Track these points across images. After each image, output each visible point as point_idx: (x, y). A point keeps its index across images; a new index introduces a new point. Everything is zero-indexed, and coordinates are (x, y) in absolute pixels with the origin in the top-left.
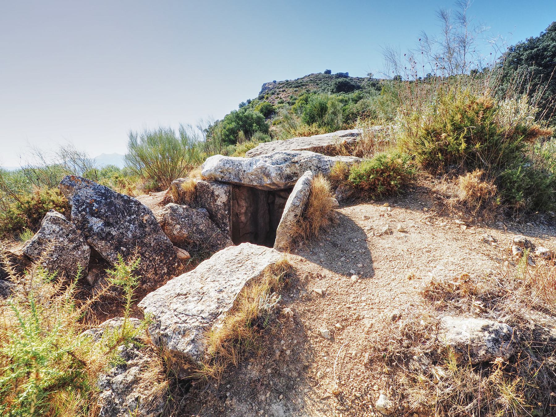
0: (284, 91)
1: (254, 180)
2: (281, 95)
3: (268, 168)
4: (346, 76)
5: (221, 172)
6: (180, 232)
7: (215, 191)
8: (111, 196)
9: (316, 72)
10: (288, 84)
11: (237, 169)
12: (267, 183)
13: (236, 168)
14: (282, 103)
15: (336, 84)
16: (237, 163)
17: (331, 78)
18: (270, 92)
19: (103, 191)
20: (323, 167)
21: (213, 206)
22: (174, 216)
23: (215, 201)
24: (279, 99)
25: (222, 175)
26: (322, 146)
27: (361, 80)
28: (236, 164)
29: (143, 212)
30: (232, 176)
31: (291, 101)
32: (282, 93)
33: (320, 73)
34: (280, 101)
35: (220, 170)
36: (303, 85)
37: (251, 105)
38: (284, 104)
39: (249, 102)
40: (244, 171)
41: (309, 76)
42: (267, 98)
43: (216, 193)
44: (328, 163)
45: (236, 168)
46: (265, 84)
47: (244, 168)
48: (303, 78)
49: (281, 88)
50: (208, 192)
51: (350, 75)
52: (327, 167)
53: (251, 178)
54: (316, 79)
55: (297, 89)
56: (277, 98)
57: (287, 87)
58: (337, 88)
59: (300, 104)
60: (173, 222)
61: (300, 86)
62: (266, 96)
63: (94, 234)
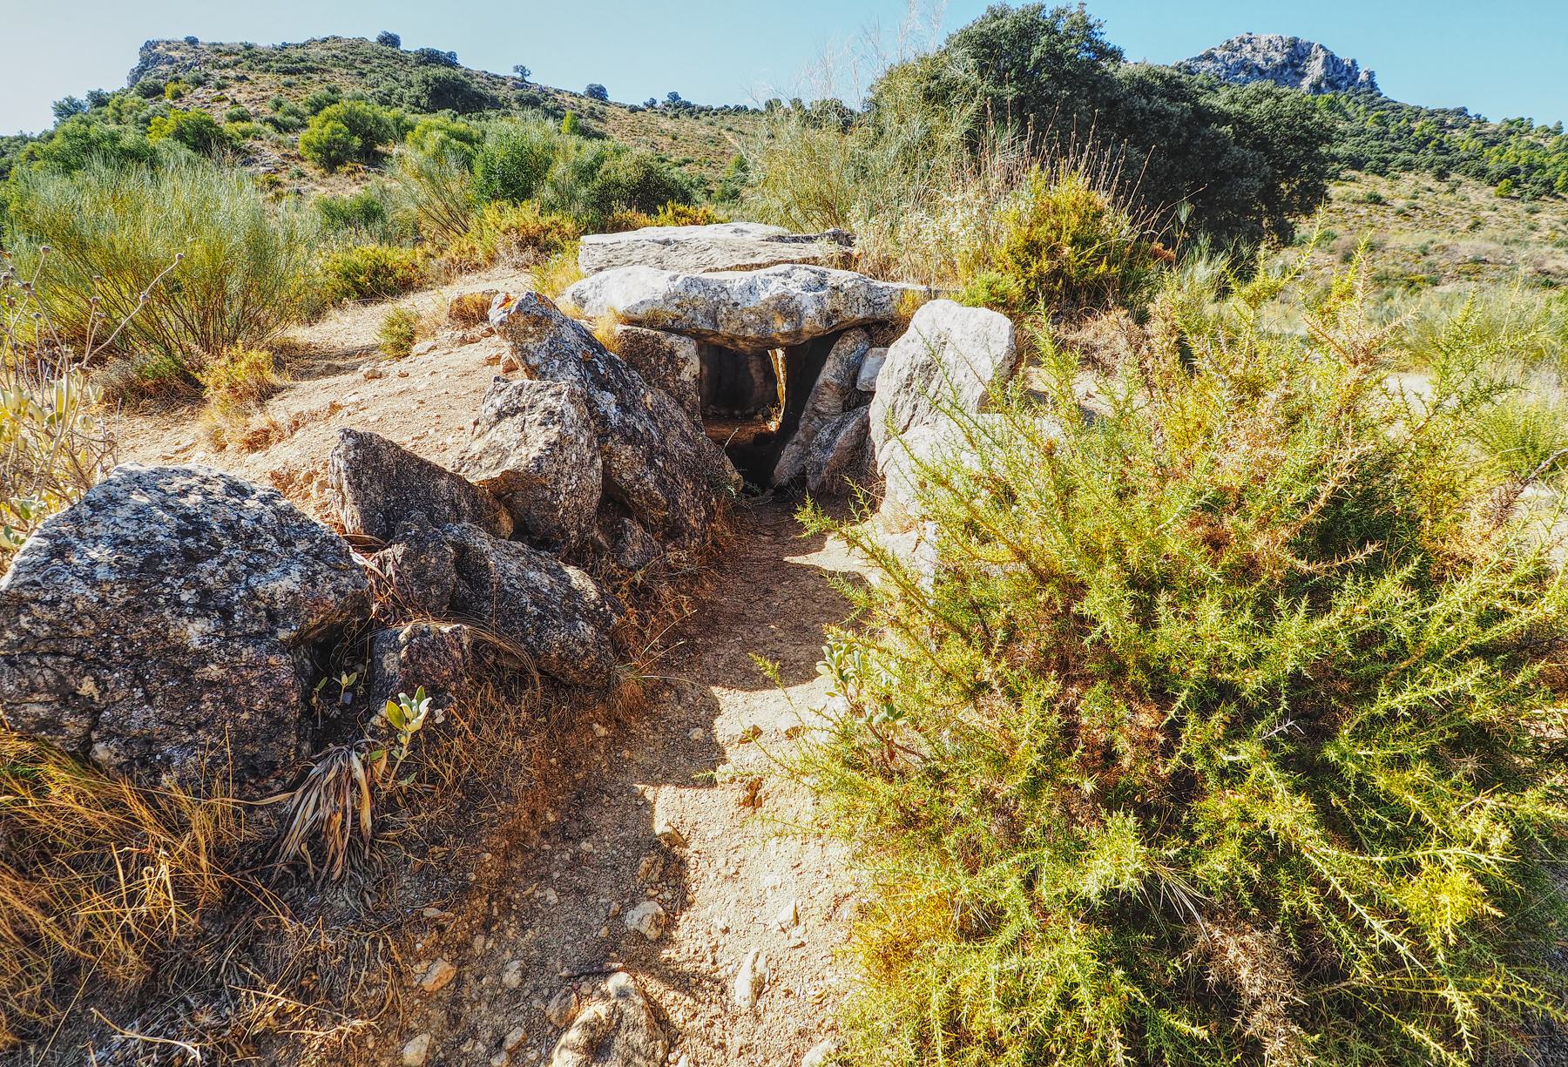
1: (753, 323)
2: (233, 91)
3: (798, 298)
4: (449, 61)
5: (678, 306)
7: (676, 348)
9: (348, 32)
10: (250, 55)
12: (782, 330)
13: (712, 298)
14: (243, 117)
15: (425, 82)
17: (403, 59)
18: (187, 76)
23: (679, 371)
24: (227, 104)
25: (679, 312)
31: (278, 116)
32: (237, 85)
33: (362, 41)
34: (234, 111)
35: (677, 301)
36: (311, 70)
37: (108, 111)
38: (255, 124)
39: (99, 100)
40: (736, 304)
41: (325, 41)
42: (178, 95)
43: (681, 354)
45: (712, 298)
46: (150, 45)
47: (736, 297)
48: (303, 46)
49: (226, 66)
50: (657, 353)
52: (884, 300)
53: (746, 319)
54: (352, 56)
55: (293, 79)
56: (220, 100)
57: (250, 68)
58: (431, 97)
59: (327, 130)
61: (300, 72)
62: (171, 87)
63: (613, 430)
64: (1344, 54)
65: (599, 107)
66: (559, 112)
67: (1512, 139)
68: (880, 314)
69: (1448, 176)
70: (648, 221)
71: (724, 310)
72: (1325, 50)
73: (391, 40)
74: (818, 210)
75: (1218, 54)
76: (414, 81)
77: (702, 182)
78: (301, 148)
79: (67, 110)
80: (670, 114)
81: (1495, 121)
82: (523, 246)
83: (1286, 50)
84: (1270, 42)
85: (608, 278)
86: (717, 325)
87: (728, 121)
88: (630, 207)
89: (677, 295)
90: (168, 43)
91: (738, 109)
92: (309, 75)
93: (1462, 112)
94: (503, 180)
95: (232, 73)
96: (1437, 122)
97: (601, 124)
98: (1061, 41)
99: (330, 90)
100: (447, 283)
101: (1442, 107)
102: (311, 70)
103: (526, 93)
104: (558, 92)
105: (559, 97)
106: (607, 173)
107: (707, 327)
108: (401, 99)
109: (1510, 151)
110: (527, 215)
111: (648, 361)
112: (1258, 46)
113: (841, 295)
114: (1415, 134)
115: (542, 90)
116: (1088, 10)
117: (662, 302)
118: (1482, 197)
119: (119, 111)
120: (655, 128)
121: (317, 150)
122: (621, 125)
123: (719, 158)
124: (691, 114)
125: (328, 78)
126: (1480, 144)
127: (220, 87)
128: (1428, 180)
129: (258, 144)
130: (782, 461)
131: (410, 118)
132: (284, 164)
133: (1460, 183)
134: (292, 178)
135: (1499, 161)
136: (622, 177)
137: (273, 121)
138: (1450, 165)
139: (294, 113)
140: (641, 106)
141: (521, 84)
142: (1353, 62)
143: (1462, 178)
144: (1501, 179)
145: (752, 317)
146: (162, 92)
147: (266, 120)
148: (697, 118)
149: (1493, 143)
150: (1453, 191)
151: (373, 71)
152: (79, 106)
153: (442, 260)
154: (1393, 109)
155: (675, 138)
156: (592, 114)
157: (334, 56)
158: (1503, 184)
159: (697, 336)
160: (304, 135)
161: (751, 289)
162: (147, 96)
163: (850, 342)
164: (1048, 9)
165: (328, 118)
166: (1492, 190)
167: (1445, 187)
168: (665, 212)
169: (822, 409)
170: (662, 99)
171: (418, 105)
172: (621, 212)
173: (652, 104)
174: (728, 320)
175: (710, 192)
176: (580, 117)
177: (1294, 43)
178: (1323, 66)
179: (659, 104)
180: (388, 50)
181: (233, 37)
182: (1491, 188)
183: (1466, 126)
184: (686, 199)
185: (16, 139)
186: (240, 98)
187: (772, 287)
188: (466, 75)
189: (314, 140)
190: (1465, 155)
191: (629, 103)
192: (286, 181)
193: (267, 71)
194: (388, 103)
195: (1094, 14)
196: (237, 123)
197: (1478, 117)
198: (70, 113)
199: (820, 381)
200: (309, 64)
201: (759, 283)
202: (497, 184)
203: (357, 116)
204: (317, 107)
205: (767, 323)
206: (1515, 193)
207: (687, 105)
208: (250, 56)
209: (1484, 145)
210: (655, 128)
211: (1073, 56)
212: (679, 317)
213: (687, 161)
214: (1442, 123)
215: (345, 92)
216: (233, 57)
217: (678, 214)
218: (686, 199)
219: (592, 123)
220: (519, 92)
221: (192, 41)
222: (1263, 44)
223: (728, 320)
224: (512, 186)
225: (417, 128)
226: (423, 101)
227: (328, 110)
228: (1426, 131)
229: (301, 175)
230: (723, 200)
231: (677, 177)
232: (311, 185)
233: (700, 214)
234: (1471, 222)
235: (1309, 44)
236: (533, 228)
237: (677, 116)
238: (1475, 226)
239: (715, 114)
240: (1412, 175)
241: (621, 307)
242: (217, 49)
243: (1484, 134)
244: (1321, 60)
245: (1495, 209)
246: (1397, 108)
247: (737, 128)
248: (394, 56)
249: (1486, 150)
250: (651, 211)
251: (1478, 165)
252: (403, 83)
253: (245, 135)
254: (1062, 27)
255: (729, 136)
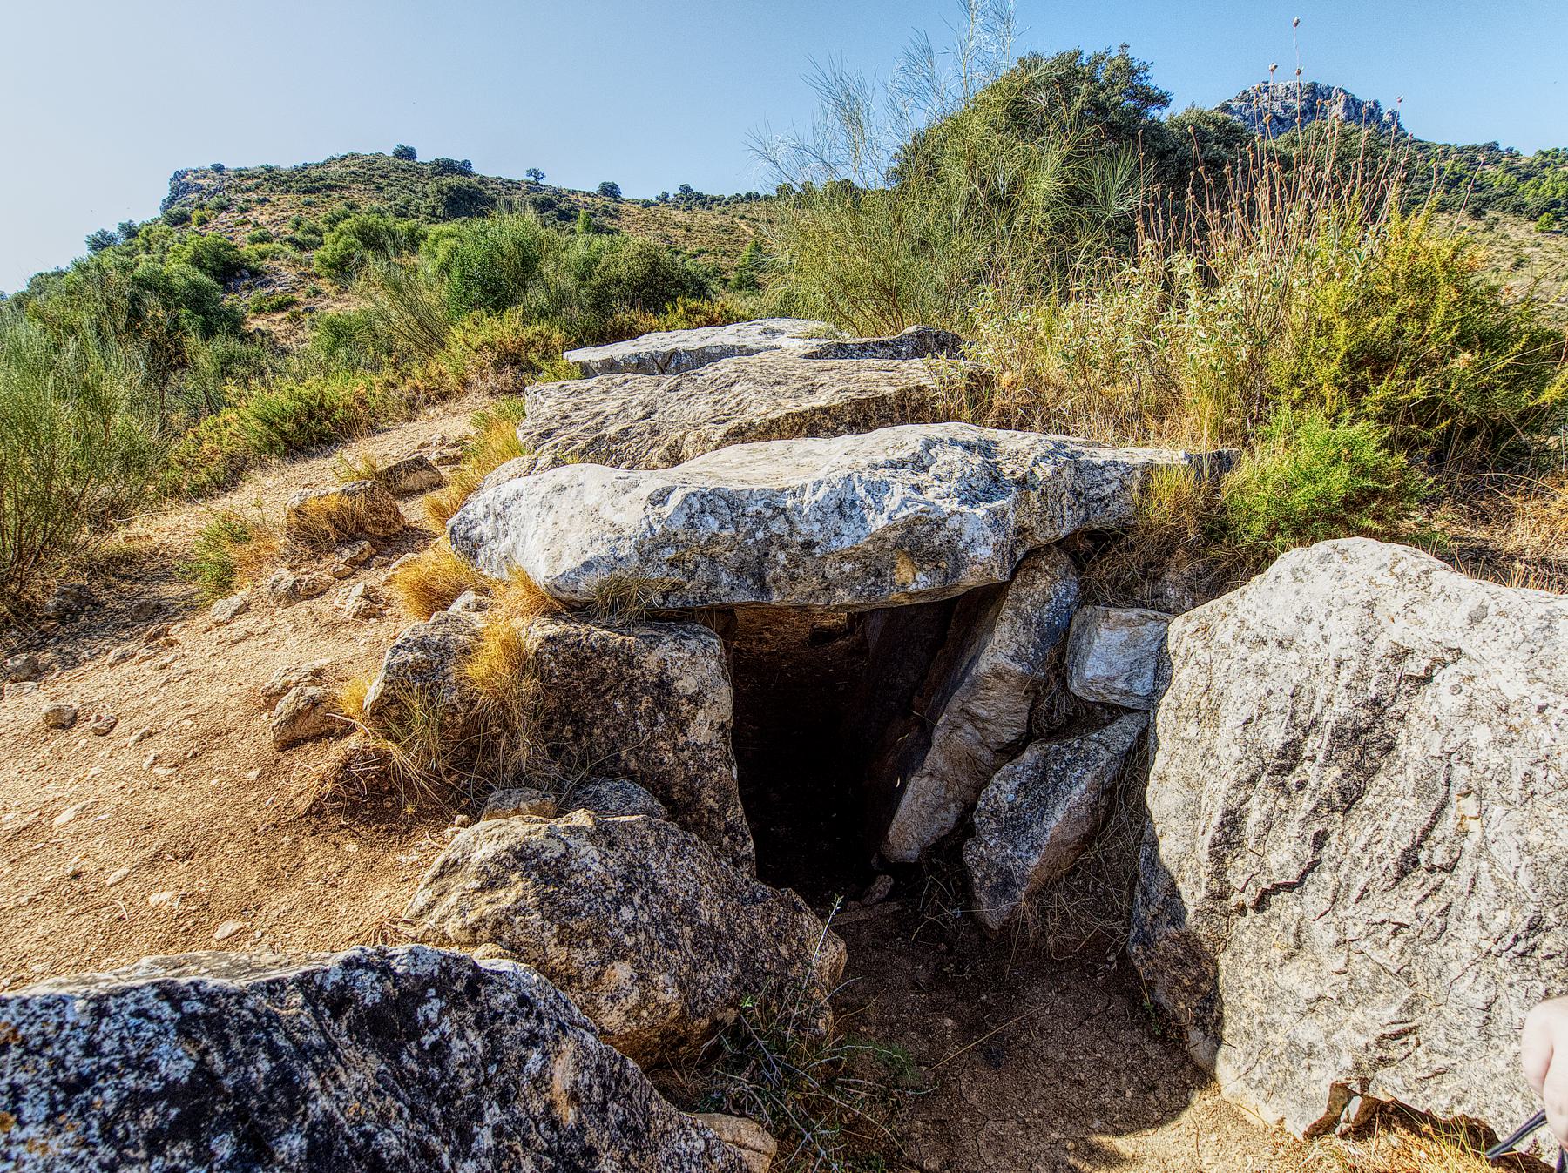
0: (265, 200)
2: (255, 214)
4: (464, 169)
6: (644, 1001)
8: (284, 1080)
9: (366, 150)
10: (272, 178)
11: (760, 535)
13: (751, 533)
14: (265, 239)
15: (440, 191)
16: (759, 506)
18: (210, 203)
19: (176, 1064)
20: (1091, 492)
21: (668, 757)
22: (572, 912)
23: (683, 726)
24: (250, 227)
25: (678, 576)
26: (884, 397)
27: (510, 186)
28: (751, 510)
29: (532, 1040)
30: (724, 578)
31: (298, 235)
32: (259, 207)
33: (379, 156)
34: (256, 233)
35: (669, 553)
36: (330, 188)
37: (138, 241)
38: (276, 245)
39: (130, 231)
40: (808, 545)
41: (343, 159)
42: (203, 222)
43: (687, 685)
44: (1112, 474)
45: (751, 533)
46: (179, 175)
48: (323, 165)
49: (248, 190)
51: (474, 168)
53: (832, 573)
54: (370, 172)
55: (313, 198)
56: (243, 224)
57: (271, 190)
59: (340, 245)
60: (578, 955)
61: (319, 190)
62: (198, 213)
64: (1364, 95)
65: (612, 205)
66: (573, 212)
67: (1547, 172)
68: (1099, 520)
69: (1485, 213)
70: (655, 322)
71: (782, 558)
72: (1345, 93)
73: (407, 153)
74: (873, 298)
75: (1233, 105)
76: (429, 192)
77: (718, 271)
78: (316, 266)
79: (100, 243)
80: (682, 206)
81: (1528, 153)
82: (499, 366)
83: (1305, 97)
84: (1288, 89)
85: (518, 495)
86: (764, 590)
87: (741, 209)
88: (632, 306)
89: (669, 540)
90: (196, 172)
91: (749, 196)
92: (329, 193)
93: (1493, 147)
94: (483, 286)
95: (254, 197)
96: (1467, 160)
97: (616, 222)
98: (1102, 88)
99: (348, 206)
100: (409, 419)
101: (1471, 143)
102: (330, 188)
103: (540, 196)
104: (572, 192)
105: (573, 198)
106: (607, 267)
107: (744, 597)
108: (417, 210)
109: (1547, 184)
110: (506, 328)
111: (608, 708)
112: (1275, 94)
113: (1033, 495)
114: (1446, 173)
115: (555, 192)
116: (1131, 53)
117: (634, 562)
118: (1522, 234)
119: (148, 241)
120: (669, 221)
121: (332, 266)
122: (635, 221)
123: (734, 247)
124: (703, 204)
125: (347, 194)
126: (1514, 179)
127: (243, 211)
128: (1463, 219)
129: (275, 264)
130: (902, 812)
131: (425, 227)
132: (300, 282)
133: (1497, 220)
134: (309, 296)
135: (1536, 195)
136: (624, 272)
137: (292, 241)
138: (1486, 202)
139: (314, 231)
140: (654, 200)
141: (535, 187)
142: (1376, 104)
143: (1500, 215)
144: (1541, 213)
145: (847, 567)
146: (189, 219)
147: (286, 240)
148: (710, 208)
149: (1528, 177)
150: (1491, 229)
151: (390, 185)
152: (112, 239)
153: (405, 389)
154: (1420, 149)
155: (688, 230)
156: (605, 213)
157: (352, 172)
158: (1543, 218)
159: (724, 620)
160: (321, 252)
161: (844, 507)
162: (175, 224)
163: (1042, 583)
164: (1085, 56)
165: (342, 234)
166: (1532, 225)
167: (1481, 225)
168: (675, 309)
169: (983, 713)
170: (673, 191)
171: (435, 215)
172: (623, 315)
173: (664, 198)
174: (792, 578)
175: (726, 281)
176: (594, 215)
177: (1313, 89)
178: (1344, 111)
179: (671, 197)
180: (404, 163)
181: (253, 161)
182: (1531, 224)
183: (1497, 162)
184: (701, 291)
185: (53, 275)
186: (262, 219)
187: (892, 502)
188: (481, 182)
189: (328, 257)
190: (1501, 191)
191: (641, 198)
192: (302, 299)
193: (287, 192)
194: (405, 216)
195: (1137, 55)
196: (257, 245)
197: (1510, 150)
198: (103, 246)
199: (983, 666)
200: (328, 182)
201: (861, 492)
202: (476, 292)
203: (371, 229)
204: (333, 222)
205: (879, 574)
206: (1557, 227)
207: (700, 196)
208: (271, 178)
209: (1518, 180)
210: (669, 221)
211: (1117, 103)
212: (677, 587)
213: (703, 252)
214: (1472, 161)
215: (363, 207)
216: (255, 181)
217: (690, 311)
218: (701, 291)
219: (607, 221)
220: (533, 195)
221: (219, 168)
222: (1280, 91)
223: (792, 578)
224: (493, 292)
225: (430, 237)
226: (440, 211)
227: (341, 225)
228: (1457, 169)
229: (317, 292)
230: (740, 288)
231: (691, 268)
232: (327, 301)
233: (718, 309)
234: (1513, 260)
235: (1328, 88)
236: (509, 340)
237: (689, 208)
238: (1518, 265)
239: (727, 203)
240: (1446, 216)
241: (541, 571)
242: (240, 174)
243: (1517, 168)
244: (1342, 104)
245: (1539, 245)
246: (1424, 148)
247: (749, 215)
248: (409, 169)
249: (1521, 185)
250: (658, 309)
251: (1515, 200)
252: (420, 195)
253: (263, 256)
254: (1102, 75)
255: (742, 224)
